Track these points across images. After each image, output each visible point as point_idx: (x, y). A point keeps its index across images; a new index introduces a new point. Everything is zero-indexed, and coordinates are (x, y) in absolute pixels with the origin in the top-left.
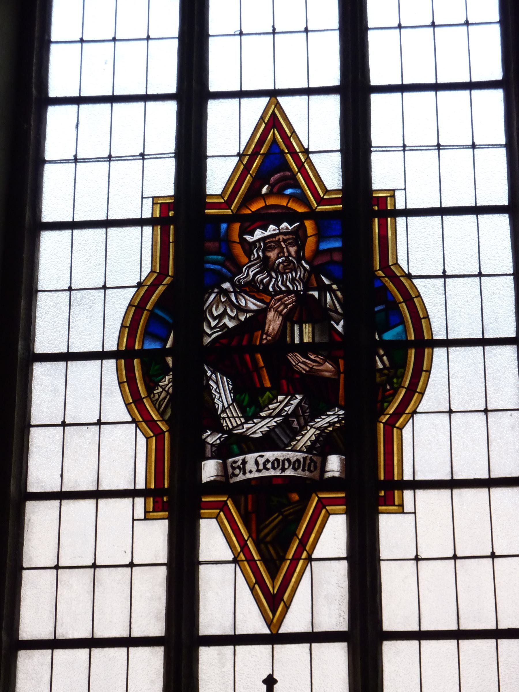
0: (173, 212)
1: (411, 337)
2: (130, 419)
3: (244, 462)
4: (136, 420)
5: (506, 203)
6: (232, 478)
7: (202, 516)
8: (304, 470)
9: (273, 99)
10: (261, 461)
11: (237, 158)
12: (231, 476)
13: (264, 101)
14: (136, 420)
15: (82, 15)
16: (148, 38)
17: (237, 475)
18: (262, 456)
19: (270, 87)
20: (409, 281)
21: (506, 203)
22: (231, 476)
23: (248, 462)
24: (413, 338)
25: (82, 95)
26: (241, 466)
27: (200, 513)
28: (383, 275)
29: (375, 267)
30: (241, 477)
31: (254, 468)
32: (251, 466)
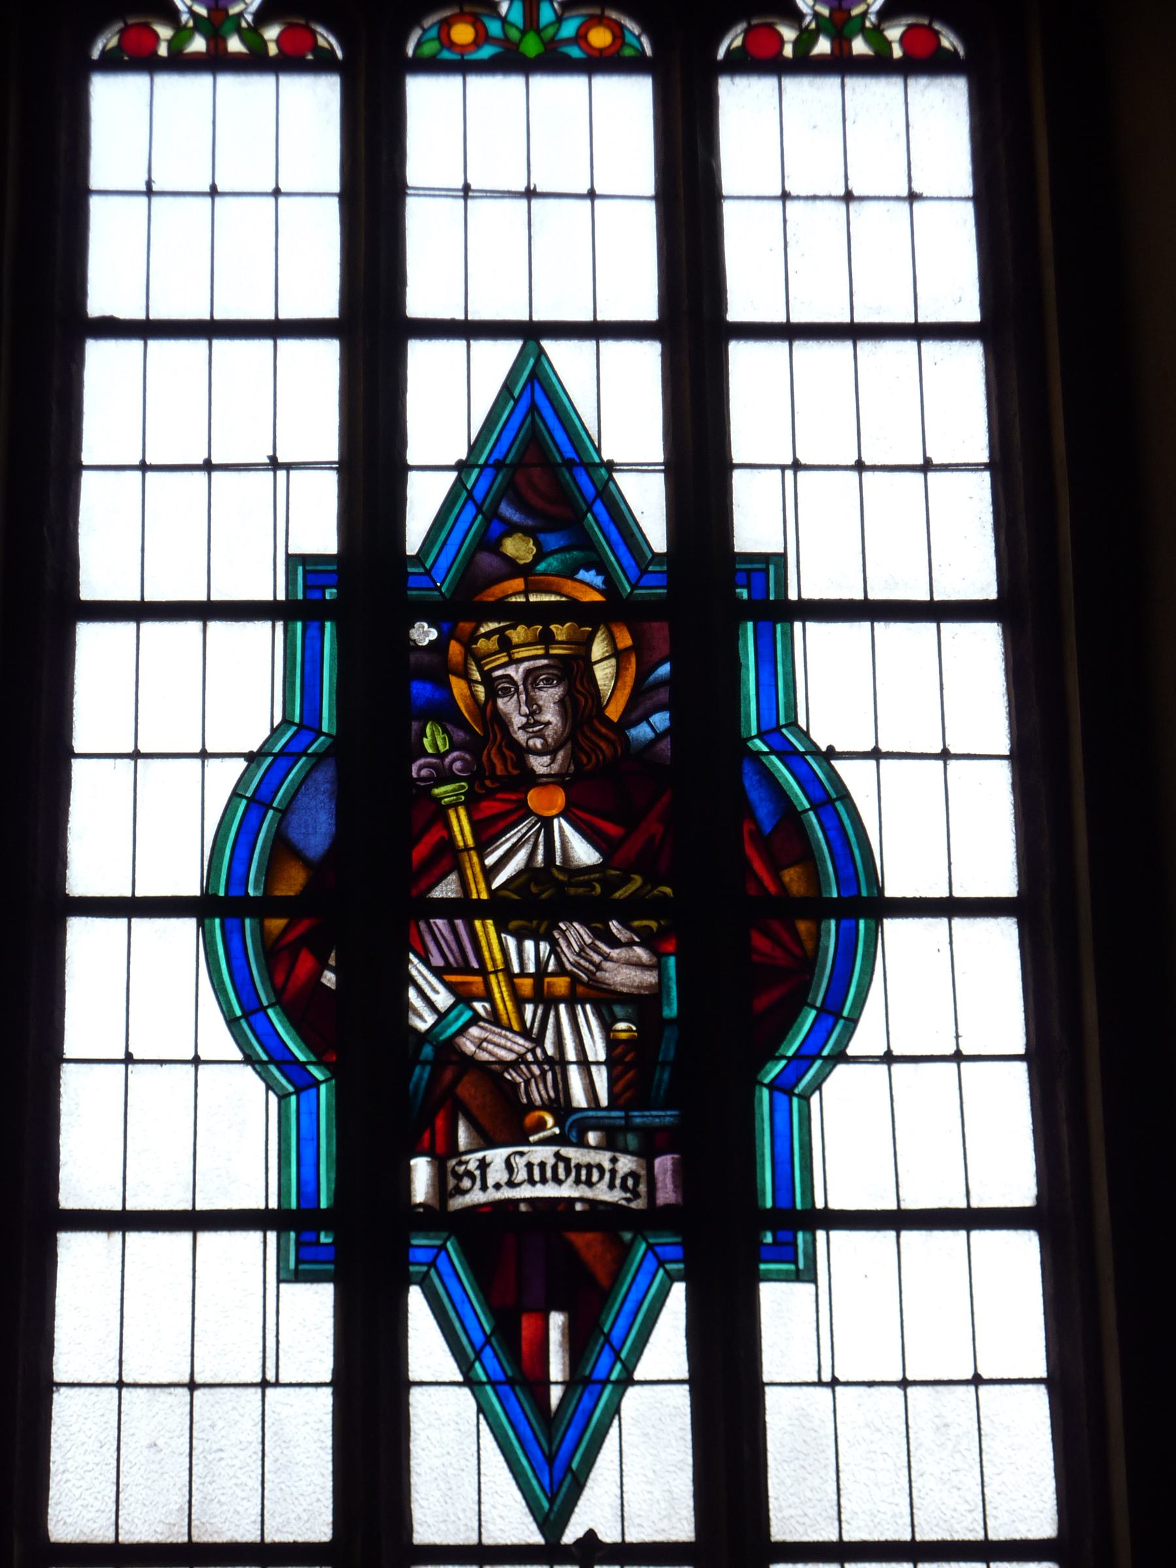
0: (335, 591)
1: (830, 892)
2: (239, 1056)
3: (483, 1165)
4: (254, 1059)
5: (991, 593)
6: (452, 1196)
7: (283, 1235)
8: (611, 1186)
9: (532, 344)
10: (520, 1162)
11: (453, 475)
12: (453, 1192)
13: (508, 350)
14: (254, 1059)
15: (745, 194)
16: (214, 192)
17: (465, 1192)
18: (522, 1154)
19: (519, 314)
20: (825, 764)
21: (991, 593)
22: (453, 1192)
23: (492, 1165)
24: (835, 895)
25: (151, 317)
26: (477, 1173)
27: (288, 1230)
28: (765, 749)
29: (334, 627)
30: (477, 1197)
31: (503, 1177)
32: (497, 1173)
